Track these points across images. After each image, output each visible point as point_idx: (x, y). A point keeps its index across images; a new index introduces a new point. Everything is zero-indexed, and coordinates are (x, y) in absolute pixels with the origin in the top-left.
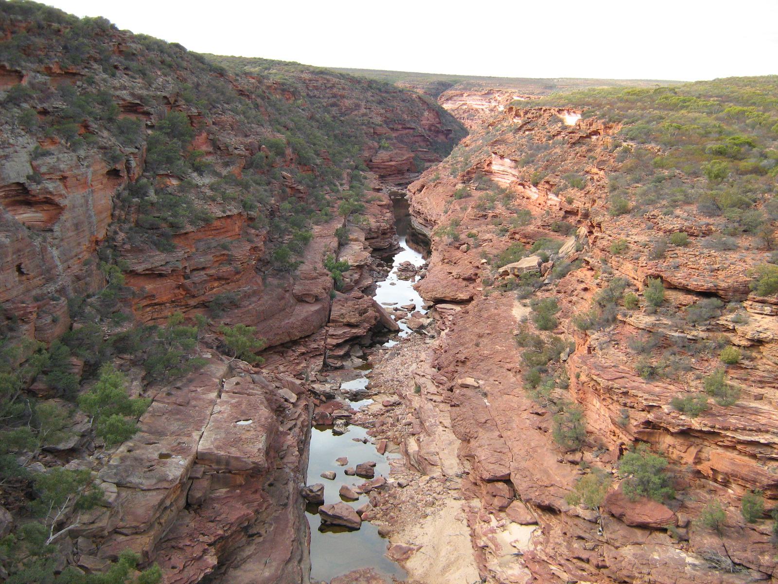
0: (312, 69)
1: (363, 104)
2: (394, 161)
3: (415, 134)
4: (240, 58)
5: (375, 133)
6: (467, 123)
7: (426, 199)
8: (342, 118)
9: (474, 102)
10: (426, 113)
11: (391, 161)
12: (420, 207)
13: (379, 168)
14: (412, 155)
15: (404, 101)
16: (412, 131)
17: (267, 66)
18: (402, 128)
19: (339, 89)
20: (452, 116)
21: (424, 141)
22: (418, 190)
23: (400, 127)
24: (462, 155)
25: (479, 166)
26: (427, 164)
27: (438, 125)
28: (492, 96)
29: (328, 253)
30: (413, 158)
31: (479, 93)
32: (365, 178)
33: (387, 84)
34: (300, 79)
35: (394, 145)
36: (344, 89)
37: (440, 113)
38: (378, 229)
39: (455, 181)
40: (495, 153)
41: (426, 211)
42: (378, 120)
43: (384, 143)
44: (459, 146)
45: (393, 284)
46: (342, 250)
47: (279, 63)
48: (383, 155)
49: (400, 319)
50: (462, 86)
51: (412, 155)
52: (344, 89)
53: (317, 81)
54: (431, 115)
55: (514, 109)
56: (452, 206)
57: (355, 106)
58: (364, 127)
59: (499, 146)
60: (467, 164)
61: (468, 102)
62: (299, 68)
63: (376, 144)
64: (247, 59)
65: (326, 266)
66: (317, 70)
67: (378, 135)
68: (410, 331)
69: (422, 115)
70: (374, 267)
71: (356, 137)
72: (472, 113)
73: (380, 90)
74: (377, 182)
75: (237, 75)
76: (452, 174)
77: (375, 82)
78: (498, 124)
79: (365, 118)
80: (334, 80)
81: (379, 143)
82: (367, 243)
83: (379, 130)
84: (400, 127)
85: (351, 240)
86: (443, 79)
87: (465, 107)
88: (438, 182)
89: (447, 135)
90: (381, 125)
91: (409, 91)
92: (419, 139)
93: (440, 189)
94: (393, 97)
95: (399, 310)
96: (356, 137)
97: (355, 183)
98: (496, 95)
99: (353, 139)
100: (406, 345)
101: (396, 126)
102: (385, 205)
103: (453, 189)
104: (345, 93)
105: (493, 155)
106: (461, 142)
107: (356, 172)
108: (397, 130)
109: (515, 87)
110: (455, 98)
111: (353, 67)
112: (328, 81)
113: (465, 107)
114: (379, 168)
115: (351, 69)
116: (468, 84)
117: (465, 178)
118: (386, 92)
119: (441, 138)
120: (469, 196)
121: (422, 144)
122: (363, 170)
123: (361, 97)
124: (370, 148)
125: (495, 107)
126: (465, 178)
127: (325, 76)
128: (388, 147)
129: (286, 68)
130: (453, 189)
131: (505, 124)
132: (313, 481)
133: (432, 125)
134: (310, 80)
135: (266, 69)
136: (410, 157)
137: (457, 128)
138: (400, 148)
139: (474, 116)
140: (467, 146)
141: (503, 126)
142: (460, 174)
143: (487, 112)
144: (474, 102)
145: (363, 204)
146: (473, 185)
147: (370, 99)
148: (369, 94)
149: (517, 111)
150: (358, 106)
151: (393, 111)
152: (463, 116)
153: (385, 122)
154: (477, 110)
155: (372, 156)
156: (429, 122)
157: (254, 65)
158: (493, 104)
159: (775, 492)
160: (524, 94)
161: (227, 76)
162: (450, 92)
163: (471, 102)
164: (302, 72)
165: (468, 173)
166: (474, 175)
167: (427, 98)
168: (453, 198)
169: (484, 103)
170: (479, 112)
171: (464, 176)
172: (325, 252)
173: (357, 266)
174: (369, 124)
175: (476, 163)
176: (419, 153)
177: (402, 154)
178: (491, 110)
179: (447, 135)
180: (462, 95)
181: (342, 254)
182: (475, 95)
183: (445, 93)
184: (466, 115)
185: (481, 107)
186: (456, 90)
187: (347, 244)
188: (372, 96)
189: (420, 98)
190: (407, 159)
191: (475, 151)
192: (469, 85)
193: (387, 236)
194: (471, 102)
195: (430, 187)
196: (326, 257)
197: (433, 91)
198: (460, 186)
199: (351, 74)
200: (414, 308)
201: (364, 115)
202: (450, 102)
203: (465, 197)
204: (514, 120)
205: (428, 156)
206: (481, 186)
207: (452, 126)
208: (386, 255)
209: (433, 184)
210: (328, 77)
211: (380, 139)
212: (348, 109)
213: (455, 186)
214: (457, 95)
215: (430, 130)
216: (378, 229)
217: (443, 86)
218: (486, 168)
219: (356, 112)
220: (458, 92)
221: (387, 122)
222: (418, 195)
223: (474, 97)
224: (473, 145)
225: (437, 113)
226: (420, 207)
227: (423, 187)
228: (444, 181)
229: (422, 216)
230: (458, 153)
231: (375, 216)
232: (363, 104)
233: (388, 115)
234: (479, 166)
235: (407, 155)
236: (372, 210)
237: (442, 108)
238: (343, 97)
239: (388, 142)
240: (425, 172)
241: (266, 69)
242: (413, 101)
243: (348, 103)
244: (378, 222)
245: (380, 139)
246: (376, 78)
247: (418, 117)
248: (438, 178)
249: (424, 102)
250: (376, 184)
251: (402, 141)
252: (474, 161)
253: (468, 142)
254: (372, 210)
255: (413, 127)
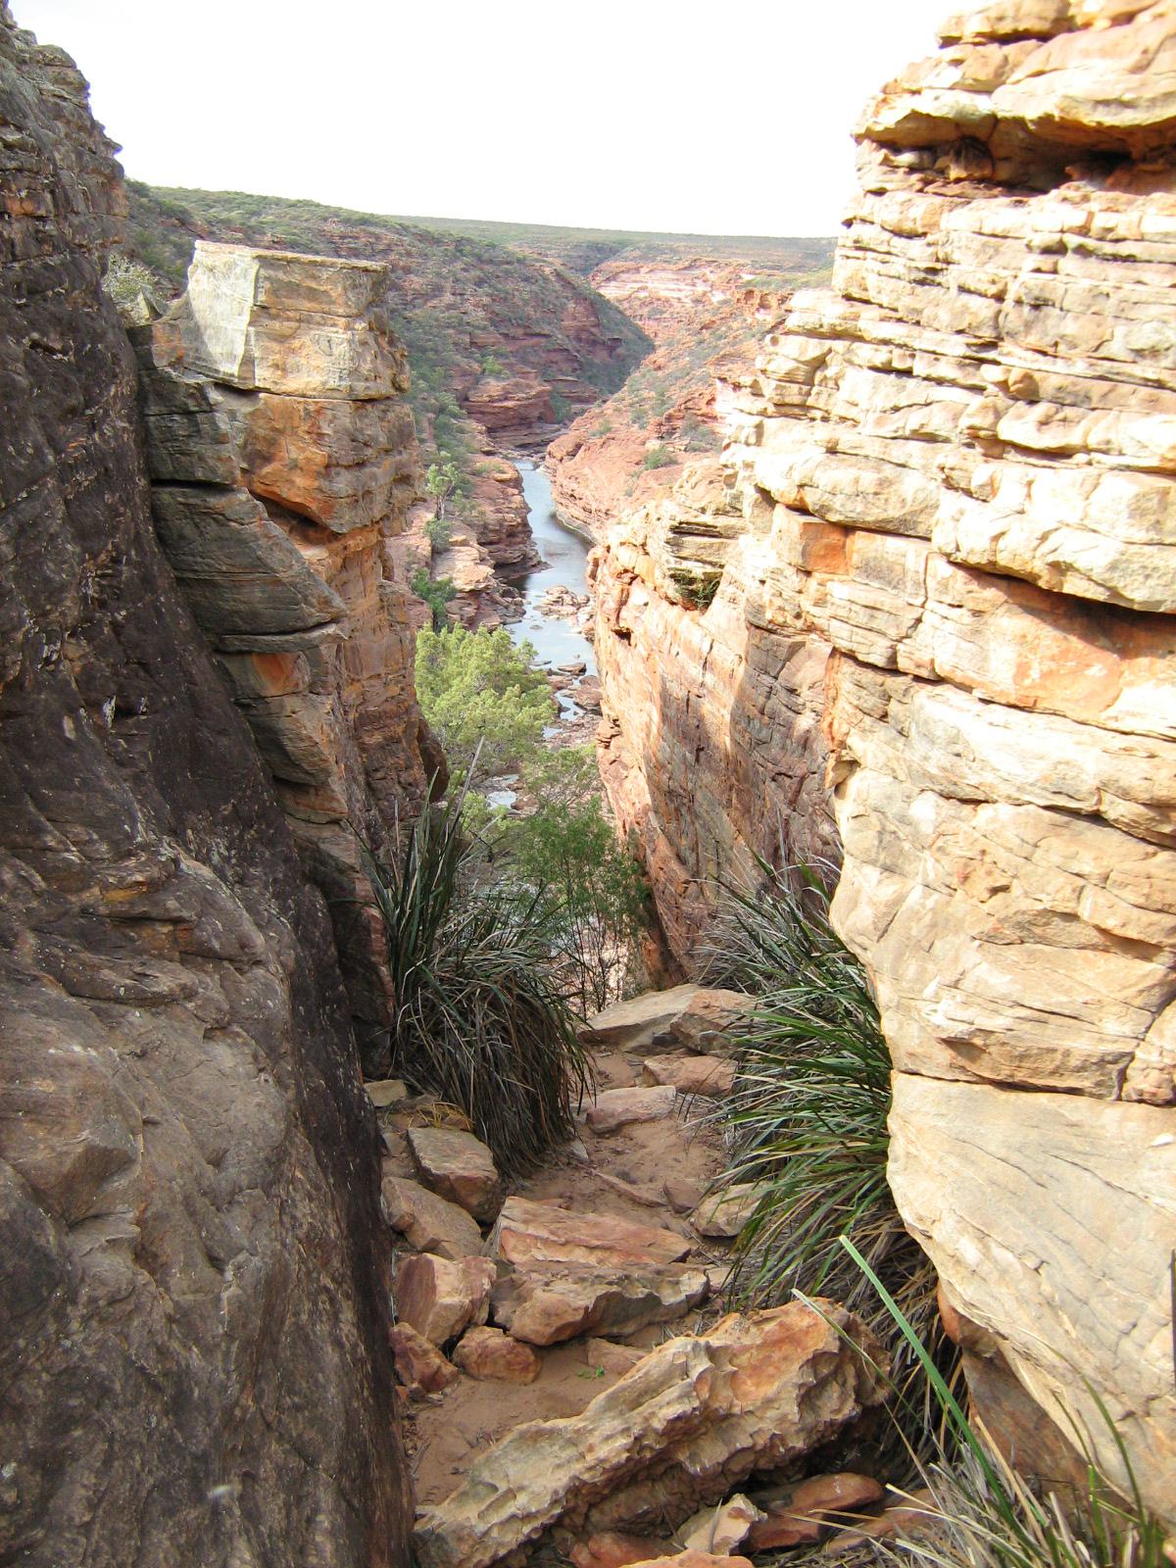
0: (344, 215)
1: (448, 285)
2: (512, 399)
3: (551, 347)
4: (196, 191)
5: (472, 343)
6: (649, 327)
7: (586, 470)
8: (408, 314)
9: (661, 284)
10: (571, 305)
11: (506, 399)
12: (575, 486)
13: (482, 413)
14: (548, 388)
15: (527, 280)
16: (543, 340)
17: (254, 208)
18: (526, 334)
19: (401, 255)
20: (620, 312)
21: (568, 360)
22: (568, 454)
23: (520, 332)
24: (651, 386)
25: (689, 404)
26: (577, 407)
27: (593, 330)
28: (697, 272)
29: (415, 566)
30: (549, 393)
31: (672, 266)
32: (462, 431)
33: (493, 247)
34: (322, 233)
35: (510, 366)
36: (409, 254)
37: (596, 305)
38: (501, 525)
39: (643, 434)
40: (723, 380)
41: (587, 493)
42: (478, 316)
43: (491, 362)
44: (643, 369)
45: (537, 627)
46: (439, 561)
47: (278, 202)
48: (493, 387)
49: (560, 689)
50: (637, 253)
51: (548, 388)
52: (409, 254)
53: (357, 238)
54: (580, 309)
55: (757, 293)
56: (641, 482)
57: (433, 290)
58: (451, 331)
59: (730, 366)
60: (663, 403)
61: (650, 285)
62: (320, 212)
63: (476, 366)
64: (213, 194)
65: (414, 589)
66: (356, 217)
67: (479, 347)
68: (581, 712)
69: (563, 307)
70: (497, 596)
71: (436, 351)
72: (657, 307)
73: (479, 258)
74: (484, 439)
75: (210, 223)
76: (634, 422)
77: (469, 241)
78: (722, 325)
79: (453, 313)
80: (391, 236)
81: (481, 363)
82: (485, 550)
83: (482, 337)
84: (520, 332)
85: (455, 544)
86: (599, 238)
87: (642, 295)
88: (607, 436)
89: (611, 349)
90: (484, 329)
91: (537, 260)
92: (557, 357)
93: (614, 450)
94: (507, 272)
95: (556, 674)
96: (436, 351)
97: (445, 438)
98: (707, 271)
99: (430, 354)
100: (578, 734)
101: (512, 331)
102: (510, 480)
103: (641, 449)
104: (412, 262)
105: (719, 384)
106: (647, 362)
107: (443, 419)
108: (514, 338)
109: (746, 255)
110: (624, 276)
111: (413, 214)
112: (378, 238)
113: (642, 295)
114: (482, 413)
115: (409, 218)
116: (650, 248)
117: (664, 429)
118: (491, 262)
119: (600, 357)
120: (672, 462)
121: (565, 367)
122: (455, 416)
123: (445, 271)
124: (465, 374)
125: (704, 294)
126: (664, 429)
127: (372, 229)
128: (500, 373)
129: (293, 212)
130: (641, 449)
131: (735, 325)
132: (798, 679)
133: (583, 329)
134: (342, 237)
135: (254, 214)
136: (543, 392)
137: (631, 336)
138: (525, 375)
139: (662, 312)
140: (659, 368)
141: (730, 328)
142: (653, 420)
143: (689, 305)
144: (661, 284)
145: (468, 477)
146: (679, 443)
147: (462, 275)
148: (459, 265)
149: (763, 297)
150: (437, 290)
151: (506, 299)
152: (640, 312)
153: (494, 324)
154: (667, 301)
155: (469, 389)
156: (575, 323)
157: (228, 206)
158: (701, 288)
159: (1053, 1565)
160: (762, 267)
161: (192, 224)
162: (612, 265)
163: (656, 284)
164: (325, 220)
165: (669, 418)
166: (679, 423)
167: (571, 276)
168: (642, 467)
169: (682, 286)
170: (671, 306)
171: (660, 424)
172: (409, 564)
173: (471, 591)
174: (460, 326)
175: (682, 400)
176: (560, 385)
177: (530, 387)
178: (697, 301)
179: (611, 349)
180: (637, 270)
181: (440, 569)
182: (664, 270)
183: (603, 266)
184: (645, 311)
185: (676, 294)
186: (626, 259)
187: (447, 550)
188: (464, 270)
189: (558, 274)
190: (539, 395)
191: (677, 379)
192: (653, 250)
193: (518, 540)
194: (656, 284)
195: (593, 448)
196: (413, 574)
197: (580, 262)
198: (654, 445)
199: (422, 226)
200: (583, 670)
201: (449, 307)
202: (613, 283)
203: (665, 465)
204: (757, 316)
205: (578, 390)
206: (695, 443)
207: (621, 332)
208: (517, 576)
209: (599, 442)
210: (377, 231)
211: (483, 356)
212: (418, 295)
213: (644, 443)
214: (628, 271)
215: (579, 340)
216: (501, 525)
217: (600, 252)
218: (705, 409)
219: (435, 302)
220: (630, 264)
221: (496, 320)
222: (569, 463)
223: (663, 275)
224: (672, 367)
225: (592, 304)
226: (575, 486)
227: (578, 446)
228: (621, 435)
229: (581, 503)
230: (640, 383)
231: (491, 499)
232: (448, 285)
233: (497, 308)
234: (689, 404)
235: (538, 387)
236: (485, 488)
237: (600, 296)
238: (407, 270)
239: (501, 361)
240: (578, 419)
241: (254, 214)
242: (546, 279)
243: (416, 282)
244: (498, 511)
245: (483, 356)
246: (474, 236)
247: (555, 313)
248: (609, 430)
249: (567, 284)
250: (483, 441)
251: (525, 361)
252: (677, 396)
253: (661, 361)
254: (485, 488)
255: (546, 332)
